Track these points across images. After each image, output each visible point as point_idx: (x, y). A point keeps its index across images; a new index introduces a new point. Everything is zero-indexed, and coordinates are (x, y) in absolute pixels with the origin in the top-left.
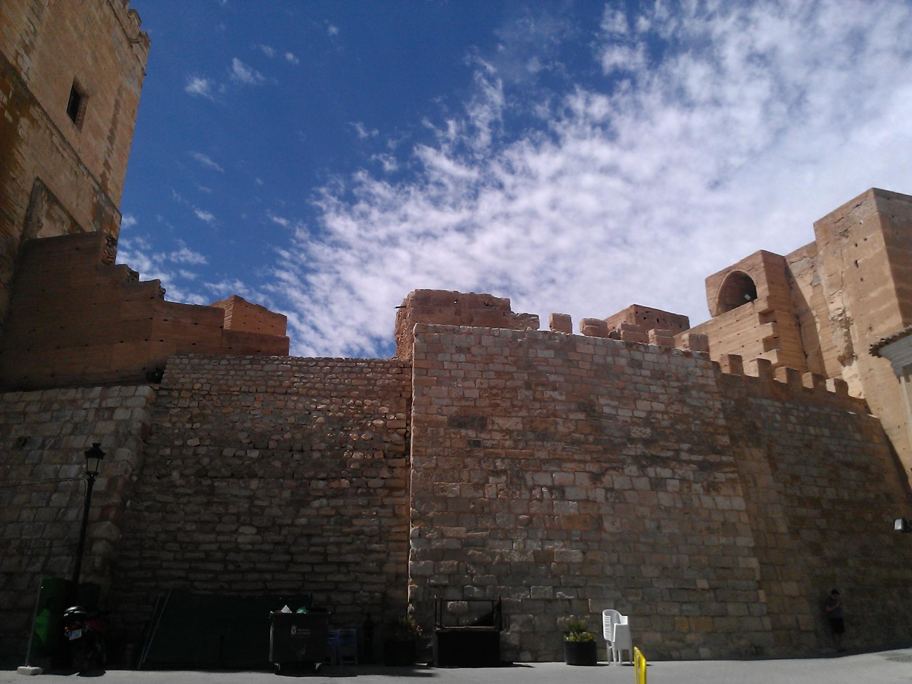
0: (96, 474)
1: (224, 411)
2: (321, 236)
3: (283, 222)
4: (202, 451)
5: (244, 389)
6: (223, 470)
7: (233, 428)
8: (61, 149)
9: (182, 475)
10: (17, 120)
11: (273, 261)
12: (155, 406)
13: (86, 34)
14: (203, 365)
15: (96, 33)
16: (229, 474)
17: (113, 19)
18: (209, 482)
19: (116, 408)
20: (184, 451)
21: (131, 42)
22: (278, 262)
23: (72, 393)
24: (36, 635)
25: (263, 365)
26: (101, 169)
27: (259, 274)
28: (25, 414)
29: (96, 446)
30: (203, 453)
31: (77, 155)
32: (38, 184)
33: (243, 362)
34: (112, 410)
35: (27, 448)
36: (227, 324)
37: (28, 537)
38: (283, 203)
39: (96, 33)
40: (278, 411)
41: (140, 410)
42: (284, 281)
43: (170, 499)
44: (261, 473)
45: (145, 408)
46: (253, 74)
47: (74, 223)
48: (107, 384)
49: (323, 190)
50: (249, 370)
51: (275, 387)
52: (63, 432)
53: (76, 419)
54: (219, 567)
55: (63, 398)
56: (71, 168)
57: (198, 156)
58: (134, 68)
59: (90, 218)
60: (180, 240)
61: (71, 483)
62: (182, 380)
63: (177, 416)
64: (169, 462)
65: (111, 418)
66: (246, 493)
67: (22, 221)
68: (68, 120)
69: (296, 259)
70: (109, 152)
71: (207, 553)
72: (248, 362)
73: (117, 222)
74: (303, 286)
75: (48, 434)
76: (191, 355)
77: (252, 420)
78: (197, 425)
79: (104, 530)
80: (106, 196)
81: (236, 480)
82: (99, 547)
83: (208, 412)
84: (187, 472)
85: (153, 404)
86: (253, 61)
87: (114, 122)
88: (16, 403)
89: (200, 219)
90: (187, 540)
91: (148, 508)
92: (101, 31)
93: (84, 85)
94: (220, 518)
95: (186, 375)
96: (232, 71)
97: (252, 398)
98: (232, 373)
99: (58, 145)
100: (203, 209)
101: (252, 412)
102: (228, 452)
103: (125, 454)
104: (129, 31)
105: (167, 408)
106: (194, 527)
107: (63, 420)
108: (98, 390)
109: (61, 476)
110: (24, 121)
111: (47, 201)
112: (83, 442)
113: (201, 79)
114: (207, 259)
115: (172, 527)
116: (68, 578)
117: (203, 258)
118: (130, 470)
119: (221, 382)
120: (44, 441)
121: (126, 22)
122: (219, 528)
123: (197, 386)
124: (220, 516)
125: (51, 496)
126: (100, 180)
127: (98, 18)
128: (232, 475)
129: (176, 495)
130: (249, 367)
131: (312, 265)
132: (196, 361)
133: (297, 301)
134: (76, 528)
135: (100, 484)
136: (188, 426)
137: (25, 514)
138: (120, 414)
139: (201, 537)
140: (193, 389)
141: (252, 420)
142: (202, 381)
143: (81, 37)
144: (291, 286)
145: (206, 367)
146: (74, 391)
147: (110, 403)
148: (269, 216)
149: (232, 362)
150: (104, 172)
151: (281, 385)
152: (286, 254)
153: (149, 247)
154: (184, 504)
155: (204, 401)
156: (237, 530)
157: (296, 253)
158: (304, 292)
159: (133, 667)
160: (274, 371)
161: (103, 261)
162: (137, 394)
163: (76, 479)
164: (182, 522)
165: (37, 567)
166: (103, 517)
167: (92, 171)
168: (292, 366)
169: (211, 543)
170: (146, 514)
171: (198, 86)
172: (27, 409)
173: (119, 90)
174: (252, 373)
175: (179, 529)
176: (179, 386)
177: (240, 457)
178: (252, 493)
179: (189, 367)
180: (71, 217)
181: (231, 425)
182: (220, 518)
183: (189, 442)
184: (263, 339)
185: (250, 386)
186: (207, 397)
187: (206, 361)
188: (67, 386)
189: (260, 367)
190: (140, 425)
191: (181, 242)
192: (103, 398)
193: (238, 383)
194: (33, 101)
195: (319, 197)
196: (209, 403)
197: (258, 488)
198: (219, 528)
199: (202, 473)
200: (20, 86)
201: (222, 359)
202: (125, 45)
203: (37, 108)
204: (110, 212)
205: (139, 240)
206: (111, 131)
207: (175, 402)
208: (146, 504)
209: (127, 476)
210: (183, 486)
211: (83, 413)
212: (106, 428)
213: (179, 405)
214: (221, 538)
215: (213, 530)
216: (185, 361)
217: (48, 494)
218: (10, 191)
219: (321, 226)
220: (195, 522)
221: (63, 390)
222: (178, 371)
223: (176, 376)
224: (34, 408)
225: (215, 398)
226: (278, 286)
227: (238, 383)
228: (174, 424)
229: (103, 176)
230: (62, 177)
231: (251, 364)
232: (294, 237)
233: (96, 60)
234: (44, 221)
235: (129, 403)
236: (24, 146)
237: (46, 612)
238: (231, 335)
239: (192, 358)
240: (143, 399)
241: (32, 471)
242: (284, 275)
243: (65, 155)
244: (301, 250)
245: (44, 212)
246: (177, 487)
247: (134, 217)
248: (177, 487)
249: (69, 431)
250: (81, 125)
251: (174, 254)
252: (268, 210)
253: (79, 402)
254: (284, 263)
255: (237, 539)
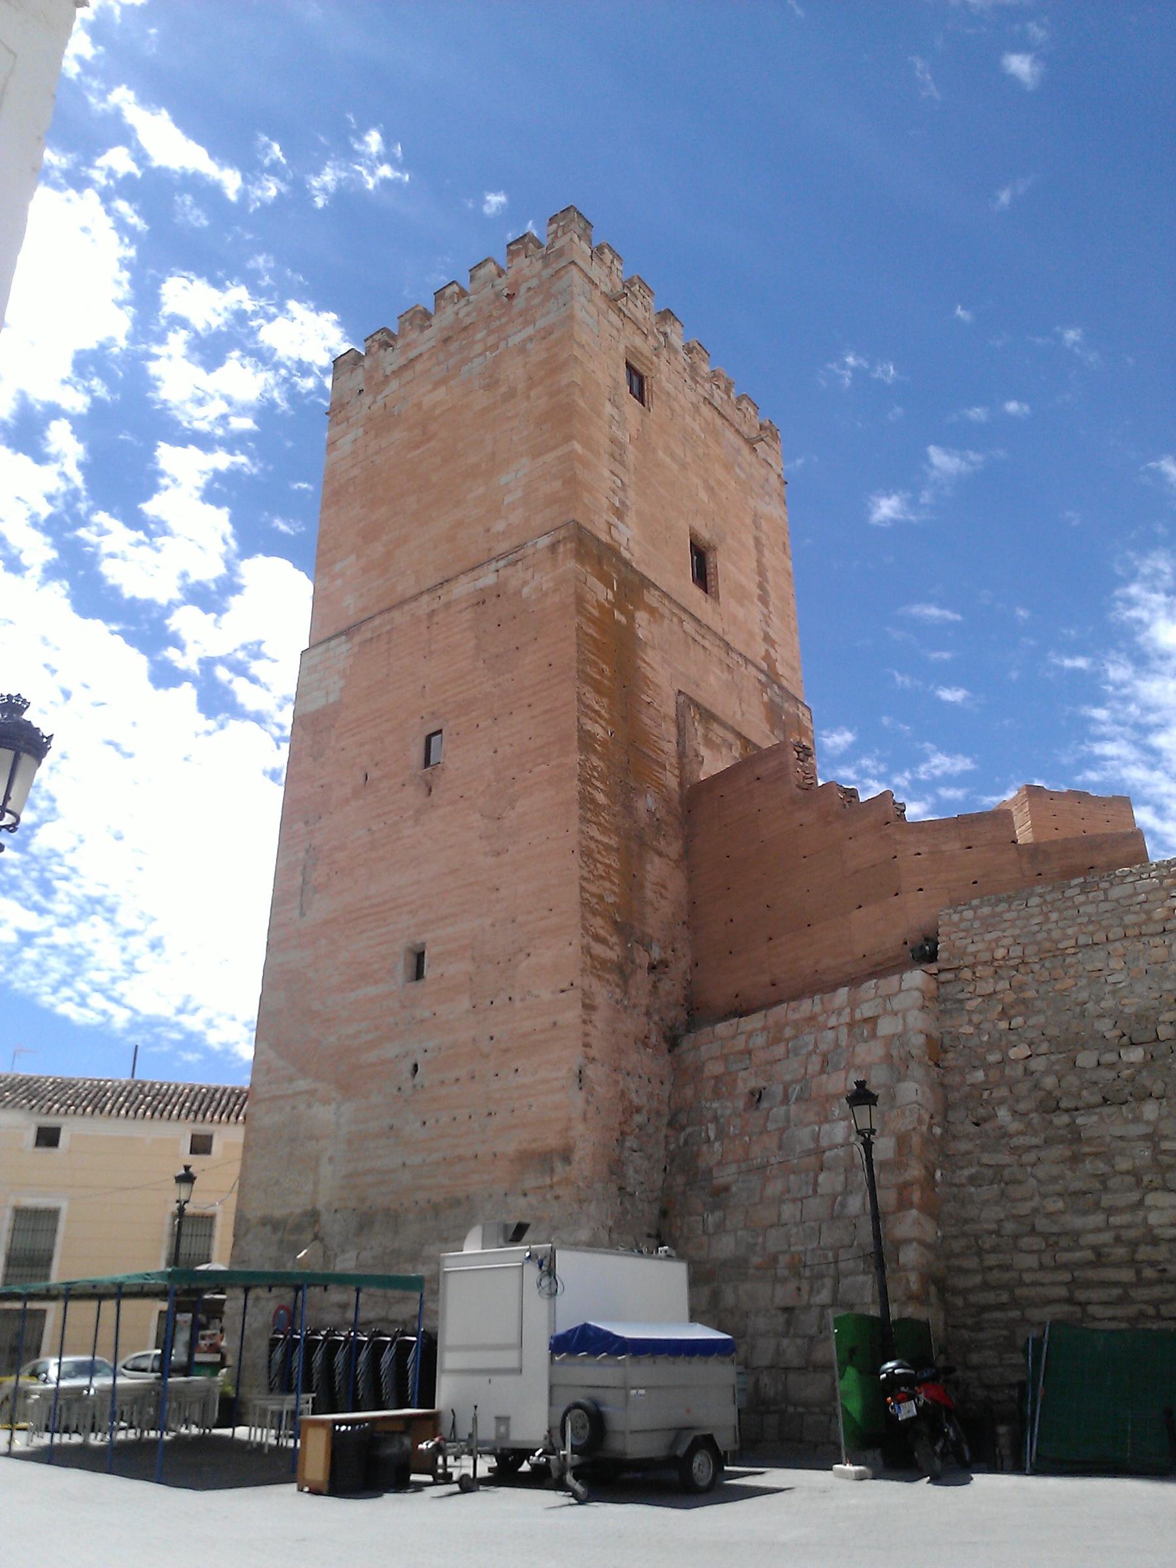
0: (872, 1131)
1: (1058, 986)
2: (1156, 664)
3: (1081, 663)
4: (1037, 1064)
5: (1083, 940)
6: (1084, 1093)
7: (1083, 1014)
8: (699, 638)
9: (1014, 1113)
10: (631, 618)
11: (1083, 730)
12: (937, 1001)
13: (689, 460)
14: (1000, 914)
15: (701, 451)
16: (1097, 1099)
17: (719, 421)
18: (1065, 1119)
19: (878, 1017)
20: (1007, 1070)
21: (750, 443)
22: (1092, 729)
23: (806, 1007)
24: (846, 1412)
25: (1105, 890)
26: (761, 648)
27: (1065, 760)
28: (749, 1052)
29: (861, 1084)
30: (1042, 1068)
31: (722, 639)
32: (681, 699)
33: (1069, 893)
34: (872, 1021)
35: (765, 1105)
36: (1024, 834)
37: (801, 1248)
38: (1073, 632)
39: (701, 451)
40: (1158, 967)
41: (915, 1012)
42: (1112, 758)
43: (1004, 1158)
44: (1158, 1088)
45: (923, 1008)
46: (962, 458)
47: (746, 742)
48: (854, 982)
49: (1134, 590)
50: (1083, 903)
51: (1139, 925)
52: (810, 1070)
53: (823, 1047)
54: (1127, 1275)
55: (796, 1016)
56: (720, 660)
57: (916, 610)
58: (767, 480)
59: (766, 727)
60: (927, 744)
61: (841, 1152)
62: (971, 948)
63: (980, 1012)
64: (986, 1094)
65: (873, 1035)
66: (1142, 1129)
67: (674, 761)
68: (698, 592)
69: (1122, 717)
70: (767, 619)
71: (1096, 1249)
72: (1077, 890)
73: (806, 723)
74: (1152, 759)
75: (788, 1077)
76: (975, 902)
77: (1114, 992)
78: (1018, 1021)
79: (909, 1225)
80: (781, 687)
81: (1113, 1109)
82: (910, 1256)
83: (1031, 994)
84: (1022, 1107)
85: (936, 999)
86: (954, 441)
87: (761, 571)
88: (734, 1037)
89: (948, 703)
90: (1055, 1229)
91: (972, 1180)
92: (708, 446)
93: (706, 535)
94: (1104, 1183)
95: (976, 939)
96: (931, 466)
97: (1103, 954)
98: (1054, 916)
99: (693, 633)
100: (947, 685)
101: (1111, 979)
102: (1086, 1059)
103: (913, 1091)
104: (745, 429)
105: (961, 1001)
106: (1060, 1205)
107: (804, 1051)
108: (843, 992)
109: (824, 1143)
110: (641, 617)
111: (700, 722)
112: (842, 1082)
113: (888, 496)
114: (975, 762)
115: (1024, 1208)
116: (874, 1311)
117: (968, 761)
118: (926, 1117)
119: (1039, 936)
120: (786, 1090)
121: (736, 417)
122: (1106, 1200)
123: (1000, 953)
124: (1103, 1179)
125: (816, 1177)
126: (764, 666)
127: (697, 428)
128: (1105, 1100)
129: (1014, 1150)
130: (1082, 898)
131: (1153, 718)
132: (986, 910)
133: (1144, 786)
134: (867, 1227)
135: (884, 1148)
136: (1003, 1025)
137: (788, 1211)
138: (887, 1027)
139: (1078, 1222)
140: (994, 959)
141: (1114, 992)
142: (1006, 942)
143: (684, 466)
144: (1126, 763)
145: (1007, 916)
146: (809, 1001)
147: (866, 1010)
148: (1056, 661)
149: (1049, 898)
150: (767, 651)
151: (1150, 919)
152: (1100, 714)
153: (882, 768)
154: (1033, 1165)
155: (1019, 977)
156: (1141, 1203)
157: (1118, 706)
158: (1152, 767)
159: (1018, 1468)
160: (1130, 896)
161: (798, 786)
162: (904, 986)
163: (847, 1144)
164: (1037, 1198)
165: (824, 1296)
166: (903, 1204)
167: (749, 656)
168: (1161, 878)
169: (1099, 1230)
170: (973, 1189)
171: (887, 508)
172: (751, 1045)
173: (754, 522)
174: (1090, 909)
175: (1035, 1211)
176: (969, 960)
177: (1111, 1066)
178: (1149, 1130)
179: (977, 924)
180: (739, 735)
181: (1078, 1009)
182: (1104, 1183)
183: (1013, 1053)
184: (1093, 844)
185: (1092, 934)
186: (1022, 969)
187: (1003, 907)
188: (797, 996)
189: (1100, 895)
190: (921, 1039)
191: (928, 746)
192: (854, 1004)
193: (1070, 931)
194: (646, 583)
195: (1130, 603)
196: (1029, 978)
197: (1160, 1118)
198: (1106, 1200)
199: (1050, 1106)
200: (623, 569)
201: (1030, 896)
202: (745, 450)
203: (652, 590)
204: (792, 710)
205: (866, 762)
206: (761, 586)
207: (971, 989)
208: (967, 1172)
209: (924, 1128)
210: (1022, 1133)
211: (830, 1035)
212: (869, 1052)
213: (978, 991)
214: (1115, 1220)
215: (1097, 1206)
216: (969, 914)
217: (812, 1174)
218: (647, 721)
219: (1149, 649)
220: (1060, 1195)
221: (792, 1004)
222: (962, 934)
223: (958, 943)
224: (759, 1040)
225: (1036, 967)
226: (1104, 769)
227: (1070, 931)
228: (977, 1026)
229: (767, 657)
230: (712, 679)
231: (1082, 892)
232: (1107, 683)
233: (711, 490)
234: (704, 751)
235: (897, 1003)
236: (650, 652)
237: (851, 1372)
238: (1034, 851)
239: (978, 907)
240: (917, 994)
241: (780, 1139)
242: (1109, 749)
243: (707, 644)
244: (1126, 700)
245: (700, 739)
246: (1011, 1136)
247: (851, 731)
248: (1011, 1136)
249: (818, 1068)
250: (717, 592)
251: (922, 768)
252: (1051, 654)
253: (821, 1019)
254: (1104, 729)
255: (1145, 1219)
